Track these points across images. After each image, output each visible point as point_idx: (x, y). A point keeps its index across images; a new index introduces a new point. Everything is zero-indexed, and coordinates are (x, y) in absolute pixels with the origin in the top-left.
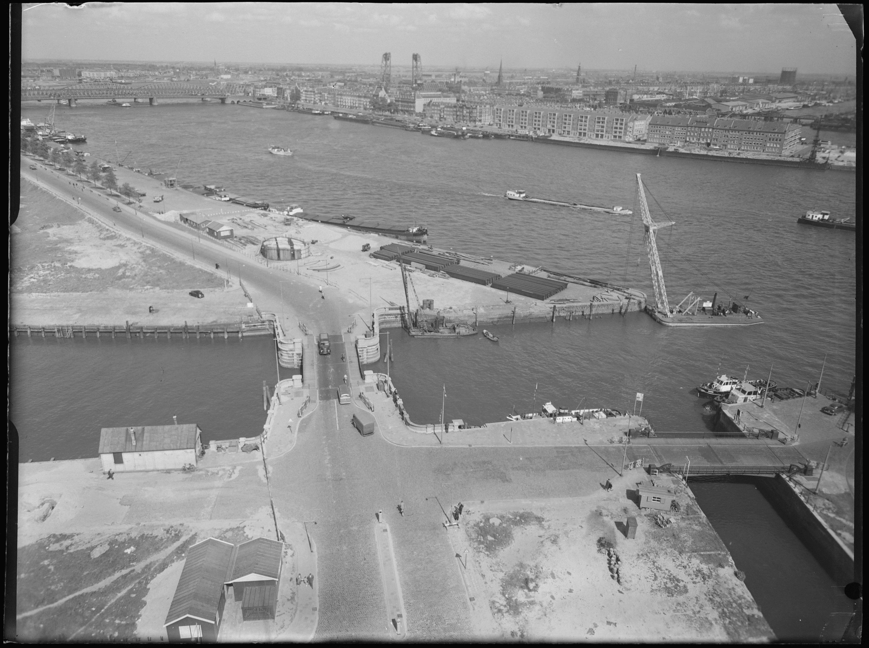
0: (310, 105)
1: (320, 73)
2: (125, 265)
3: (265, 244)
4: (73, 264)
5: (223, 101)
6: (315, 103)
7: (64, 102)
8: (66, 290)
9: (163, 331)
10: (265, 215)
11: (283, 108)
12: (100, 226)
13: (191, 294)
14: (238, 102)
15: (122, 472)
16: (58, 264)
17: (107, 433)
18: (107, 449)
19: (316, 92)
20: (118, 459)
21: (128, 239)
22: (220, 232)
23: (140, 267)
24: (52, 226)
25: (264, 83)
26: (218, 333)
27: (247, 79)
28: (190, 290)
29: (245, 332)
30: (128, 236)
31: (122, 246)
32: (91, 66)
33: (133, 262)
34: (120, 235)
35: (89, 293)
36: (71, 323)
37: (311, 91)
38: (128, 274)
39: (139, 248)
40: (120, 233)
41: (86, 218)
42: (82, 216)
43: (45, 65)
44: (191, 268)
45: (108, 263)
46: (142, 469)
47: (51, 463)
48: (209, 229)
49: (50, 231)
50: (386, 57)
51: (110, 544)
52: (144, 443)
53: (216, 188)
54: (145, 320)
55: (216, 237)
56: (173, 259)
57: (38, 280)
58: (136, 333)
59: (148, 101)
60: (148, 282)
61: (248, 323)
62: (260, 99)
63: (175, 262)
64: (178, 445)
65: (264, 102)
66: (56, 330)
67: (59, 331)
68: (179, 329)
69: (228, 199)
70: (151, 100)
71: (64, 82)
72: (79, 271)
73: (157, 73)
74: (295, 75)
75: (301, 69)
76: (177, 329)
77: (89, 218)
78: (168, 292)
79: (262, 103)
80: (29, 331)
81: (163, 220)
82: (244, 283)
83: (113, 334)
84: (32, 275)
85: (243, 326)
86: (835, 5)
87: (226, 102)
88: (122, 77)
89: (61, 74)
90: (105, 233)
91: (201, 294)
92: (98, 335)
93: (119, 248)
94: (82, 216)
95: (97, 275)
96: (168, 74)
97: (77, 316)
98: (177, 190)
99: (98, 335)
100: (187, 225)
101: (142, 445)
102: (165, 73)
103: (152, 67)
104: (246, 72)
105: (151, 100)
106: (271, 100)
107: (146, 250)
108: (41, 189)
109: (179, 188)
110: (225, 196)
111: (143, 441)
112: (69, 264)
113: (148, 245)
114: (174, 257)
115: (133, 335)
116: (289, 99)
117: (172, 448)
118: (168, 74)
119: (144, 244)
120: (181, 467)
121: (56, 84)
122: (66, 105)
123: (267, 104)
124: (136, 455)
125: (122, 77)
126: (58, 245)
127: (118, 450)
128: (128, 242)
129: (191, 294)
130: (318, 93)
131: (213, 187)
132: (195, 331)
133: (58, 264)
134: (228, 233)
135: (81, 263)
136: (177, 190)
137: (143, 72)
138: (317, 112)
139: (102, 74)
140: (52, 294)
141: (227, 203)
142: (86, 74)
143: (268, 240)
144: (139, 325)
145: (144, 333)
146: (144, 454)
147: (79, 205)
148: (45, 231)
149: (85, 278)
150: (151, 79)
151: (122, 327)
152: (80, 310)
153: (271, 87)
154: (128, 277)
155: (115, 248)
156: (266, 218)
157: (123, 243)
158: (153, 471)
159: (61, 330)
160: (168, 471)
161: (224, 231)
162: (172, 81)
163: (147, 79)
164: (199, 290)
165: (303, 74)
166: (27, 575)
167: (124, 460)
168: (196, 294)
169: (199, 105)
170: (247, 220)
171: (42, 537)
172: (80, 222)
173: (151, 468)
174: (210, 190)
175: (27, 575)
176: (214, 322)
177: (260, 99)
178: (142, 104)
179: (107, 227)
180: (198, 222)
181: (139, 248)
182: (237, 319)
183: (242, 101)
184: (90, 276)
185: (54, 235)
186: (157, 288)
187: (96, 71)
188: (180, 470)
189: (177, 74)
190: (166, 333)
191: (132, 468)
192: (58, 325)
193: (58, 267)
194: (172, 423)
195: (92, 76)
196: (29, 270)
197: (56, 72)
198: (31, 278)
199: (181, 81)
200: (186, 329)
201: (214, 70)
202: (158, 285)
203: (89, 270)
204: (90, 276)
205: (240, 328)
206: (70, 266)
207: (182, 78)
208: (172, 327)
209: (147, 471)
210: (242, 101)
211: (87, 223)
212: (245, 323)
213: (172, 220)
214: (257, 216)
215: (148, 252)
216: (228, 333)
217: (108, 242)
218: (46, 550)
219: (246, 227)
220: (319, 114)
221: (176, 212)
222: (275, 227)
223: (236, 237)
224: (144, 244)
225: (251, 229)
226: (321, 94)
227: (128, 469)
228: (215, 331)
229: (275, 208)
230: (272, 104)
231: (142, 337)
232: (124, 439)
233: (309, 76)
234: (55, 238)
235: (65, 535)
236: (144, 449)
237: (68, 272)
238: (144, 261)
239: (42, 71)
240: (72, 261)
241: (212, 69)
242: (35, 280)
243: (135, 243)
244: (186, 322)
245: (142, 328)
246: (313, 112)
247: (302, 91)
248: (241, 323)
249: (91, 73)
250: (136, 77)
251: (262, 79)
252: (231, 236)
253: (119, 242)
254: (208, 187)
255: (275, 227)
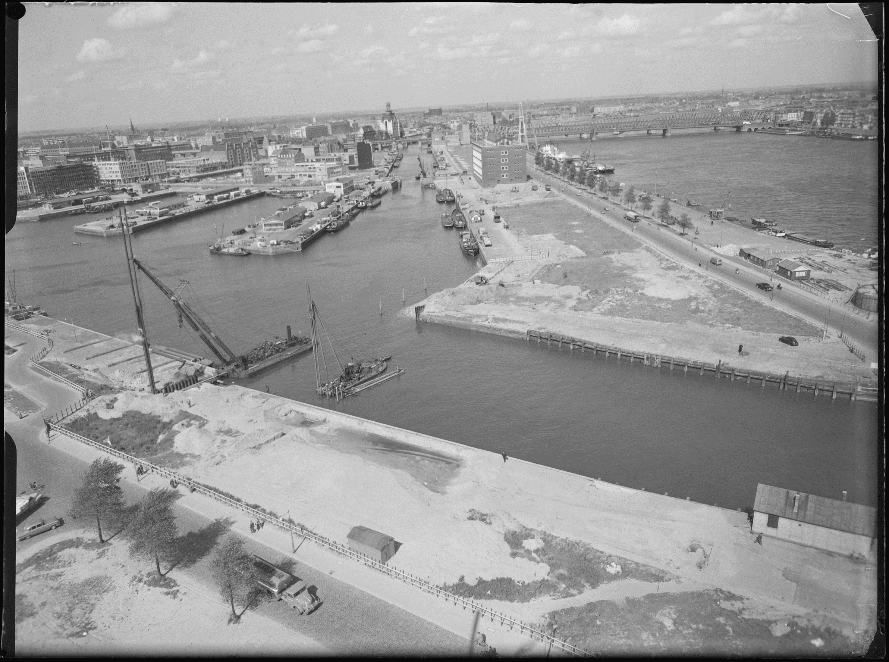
0: (848, 130)
1: (846, 93)
2: (696, 298)
3: (861, 291)
4: (643, 291)
5: (739, 129)
6: (853, 127)
7: (585, 136)
8: (644, 317)
9: (757, 377)
10: (841, 257)
11: (812, 134)
12: (659, 255)
13: (783, 340)
14: (756, 129)
15: (773, 537)
16: (630, 291)
17: (763, 491)
18: (763, 508)
19: (857, 114)
20: (773, 522)
21: (692, 272)
22: (795, 272)
23: (712, 302)
24: (614, 253)
25: (783, 108)
26: (823, 390)
27: (760, 105)
28: (781, 336)
29: (859, 395)
30: (692, 268)
31: (687, 278)
32: (600, 102)
33: (703, 296)
34: (682, 267)
35: (669, 323)
36: (658, 352)
37: (850, 114)
38: (702, 308)
39: (705, 282)
40: (682, 264)
41: (643, 246)
42: (639, 245)
43: (562, 104)
44: (770, 310)
45: (677, 294)
46: (797, 541)
47: (687, 502)
48: (780, 267)
49: (612, 256)
50: (389, 105)
51: (791, 624)
52: (808, 513)
53: (767, 222)
54: (735, 362)
55: (789, 278)
56: (747, 298)
57: (617, 305)
58: (727, 374)
59: (661, 132)
60: (727, 320)
61: (866, 386)
62: (782, 125)
63: (750, 301)
64: (851, 527)
65: (787, 129)
66: (645, 357)
67: (648, 358)
68: (777, 378)
69: (783, 234)
70: (665, 131)
71: (580, 118)
72: (650, 299)
73: (662, 105)
74: (814, 97)
75: (821, 90)
76: (773, 378)
77: (646, 247)
78: (754, 334)
79: (784, 130)
80: (619, 354)
81: (722, 253)
82: (845, 335)
83: (702, 370)
84: (610, 299)
85: (859, 389)
86: (856, 4)
87: (742, 130)
88: (631, 111)
89: (577, 111)
90: (665, 263)
91: (796, 341)
92: (686, 369)
93: (683, 280)
94: (639, 245)
95: (670, 306)
96: (673, 105)
97: (664, 346)
98: (722, 222)
99: (686, 369)
100: (748, 261)
101: (805, 514)
102: (670, 104)
103: (655, 99)
104: (756, 98)
105: (665, 131)
106: (795, 126)
107: (713, 284)
108: (594, 216)
109: (724, 221)
110: (781, 232)
111: (806, 510)
112: (640, 291)
113: (715, 279)
114: (747, 295)
115: (723, 375)
116: (819, 124)
117: (844, 528)
118: (673, 105)
119: (710, 278)
120: (847, 553)
121: (573, 120)
122: (587, 139)
123: (792, 130)
124: (795, 524)
125: (631, 111)
126: (624, 272)
127: (775, 512)
128: (691, 274)
129: (783, 340)
130: (860, 115)
131: (763, 221)
132: (796, 384)
133: (630, 291)
134: (803, 274)
135: (650, 291)
136: (722, 222)
137: (649, 105)
138: (858, 137)
139: (612, 109)
140: (634, 320)
141: (782, 239)
142: (598, 110)
143: (863, 287)
144: (731, 365)
145: (735, 375)
146: (805, 526)
147: (633, 233)
148: (608, 256)
149: (659, 307)
150: (657, 111)
151: (713, 365)
152: (664, 341)
153: (796, 111)
154: (703, 311)
155: (678, 279)
156: (840, 260)
157: (686, 275)
158: (810, 547)
159: (650, 358)
160: (830, 554)
161: (801, 271)
162: (677, 111)
163: (653, 111)
164: (793, 337)
165: (824, 96)
166: (705, 628)
167: (779, 525)
168: (788, 341)
169: (710, 134)
170: (819, 260)
171: (708, 587)
172: (637, 250)
173: (809, 544)
174: (760, 223)
175: (705, 628)
176: (819, 377)
177: (782, 125)
178: (655, 135)
179: (667, 258)
180: (766, 260)
181: (705, 282)
182: (849, 378)
183: (760, 128)
184: (663, 305)
185: (618, 261)
186: (739, 328)
187: (606, 106)
188: (846, 557)
189: (684, 105)
190: (761, 380)
191: (786, 537)
192: (647, 352)
193: (630, 293)
194: (840, 498)
195: (602, 111)
196: (605, 294)
197: (574, 110)
198: (610, 301)
199: (686, 111)
200: (785, 380)
201: (720, 97)
202: (739, 325)
203: (660, 300)
204: (663, 305)
205: (854, 390)
206: (641, 294)
207: (688, 108)
208: (768, 374)
209: (803, 546)
210: (760, 128)
211: (644, 252)
212: (863, 385)
213: (731, 254)
214: (827, 256)
215: (716, 287)
216: (837, 392)
217: (671, 272)
218: (718, 605)
219: (821, 269)
220: (861, 139)
221: (735, 246)
222: (858, 271)
223: (812, 279)
224: (710, 278)
225: (828, 271)
226: (863, 115)
227: (780, 536)
228: (821, 387)
229: (849, 249)
230: (796, 131)
231: (732, 379)
232: (783, 501)
233: (831, 97)
234: (619, 265)
235: (734, 595)
236: (807, 520)
237: (640, 299)
238: (715, 296)
239: (563, 109)
240: (643, 289)
241: (717, 97)
242: (614, 304)
243: (700, 276)
244: (788, 372)
245: (733, 370)
246: (853, 137)
247: (837, 114)
248: (857, 384)
249: (603, 109)
250: (643, 110)
251: (781, 103)
252: (807, 278)
253: (682, 274)
254: (758, 220)
255: (858, 271)
